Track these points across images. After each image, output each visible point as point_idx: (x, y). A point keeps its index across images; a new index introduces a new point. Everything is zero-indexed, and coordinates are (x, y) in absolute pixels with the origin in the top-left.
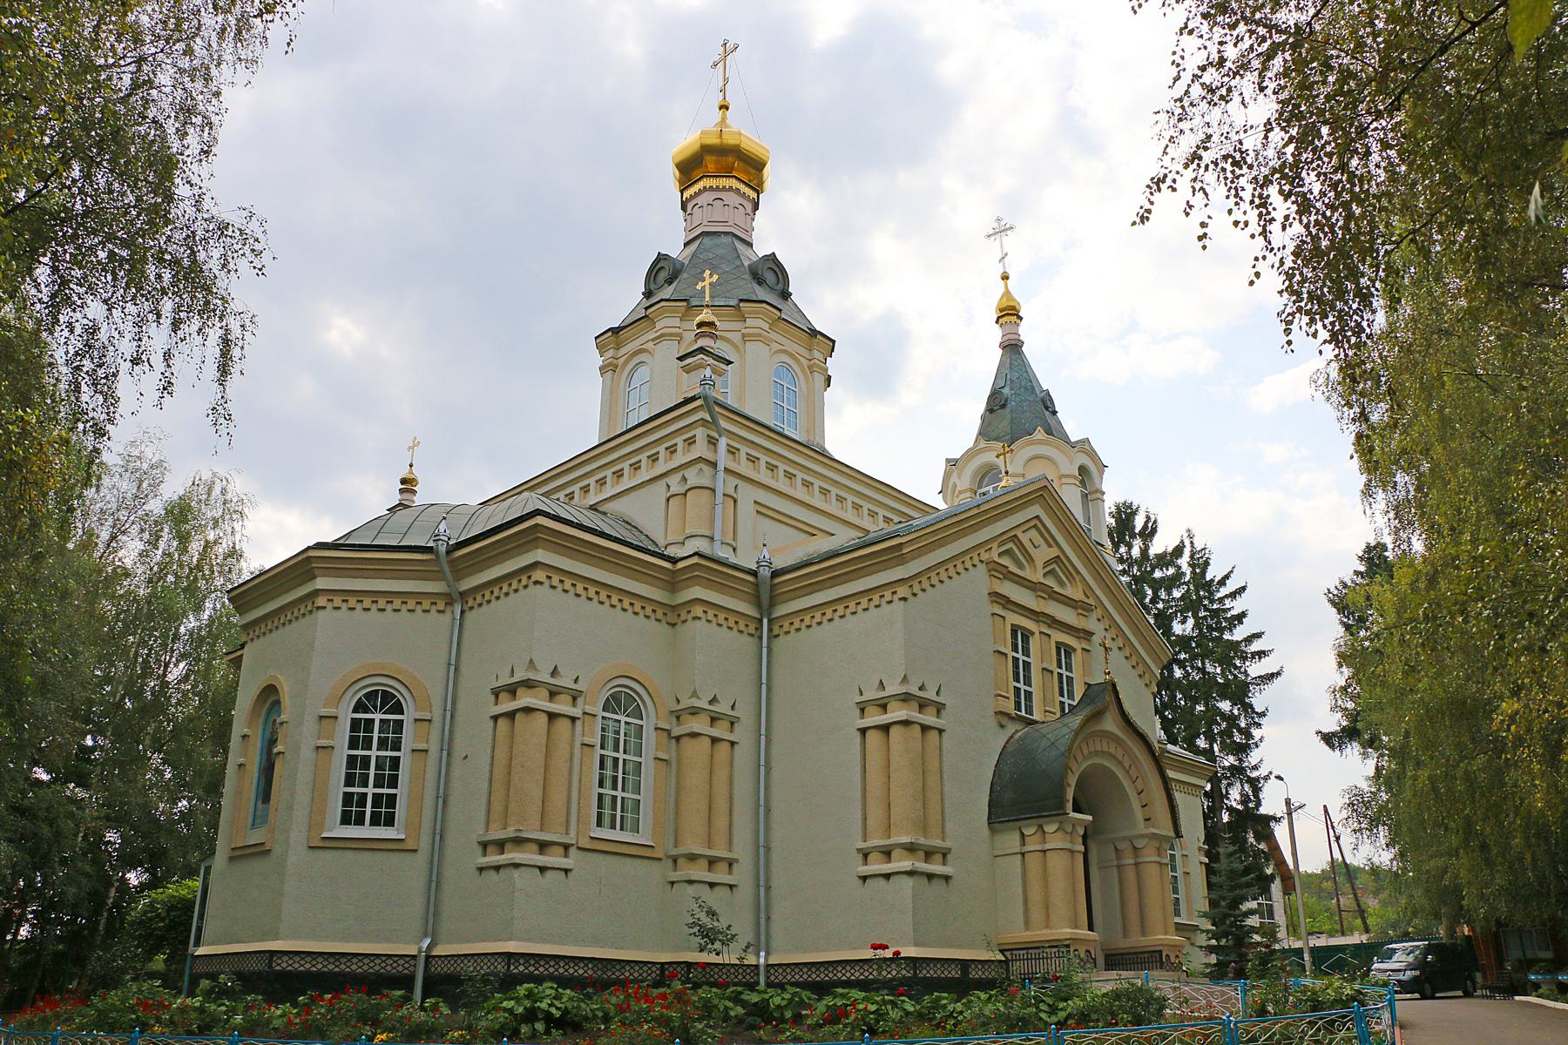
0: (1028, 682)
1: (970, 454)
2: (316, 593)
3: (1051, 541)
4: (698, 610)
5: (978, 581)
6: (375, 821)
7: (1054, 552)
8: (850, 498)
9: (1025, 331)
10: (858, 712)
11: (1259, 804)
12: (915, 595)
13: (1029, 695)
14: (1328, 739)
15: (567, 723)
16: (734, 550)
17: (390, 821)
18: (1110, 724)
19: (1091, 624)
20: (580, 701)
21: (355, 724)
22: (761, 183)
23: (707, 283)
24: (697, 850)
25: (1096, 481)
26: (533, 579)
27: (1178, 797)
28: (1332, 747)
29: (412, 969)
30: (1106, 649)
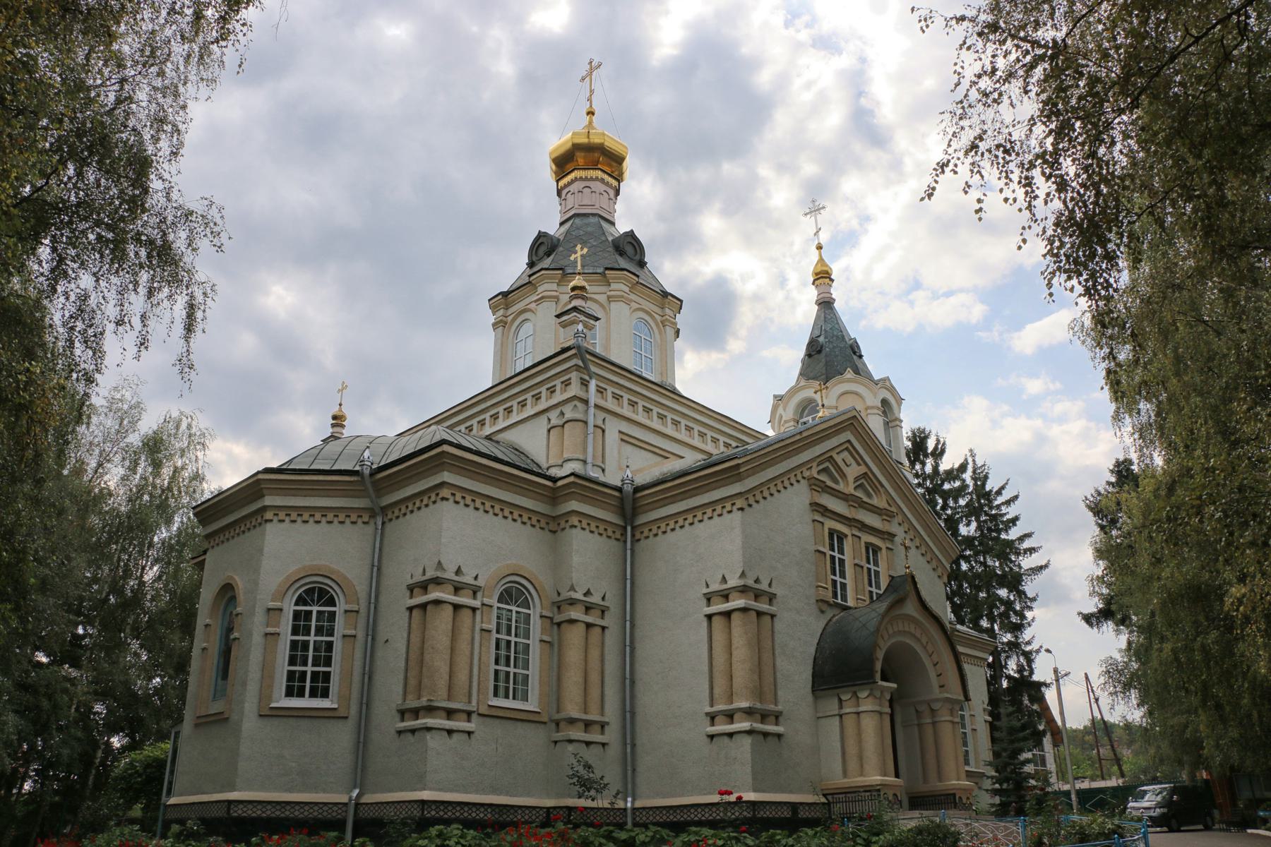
0: (843, 575)
1: (793, 391)
2: (265, 508)
3: (860, 461)
4: (574, 520)
5: (797, 498)
7: (863, 469)
8: (697, 428)
9: (836, 292)
10: (705, 601)
11: (1032, 672)
12: (750, 506)
13: (844, 586)
14: (1088, 619)
15: (469, 612)
16: (603, 470)
17: (325, 694)
18: (910, 608)
19: (894, 528)
20: (479, 595)
21: (297, 615)
25: (896, 411)
27: (966, 667)
28: (1091, 625)
30: (906, 548)
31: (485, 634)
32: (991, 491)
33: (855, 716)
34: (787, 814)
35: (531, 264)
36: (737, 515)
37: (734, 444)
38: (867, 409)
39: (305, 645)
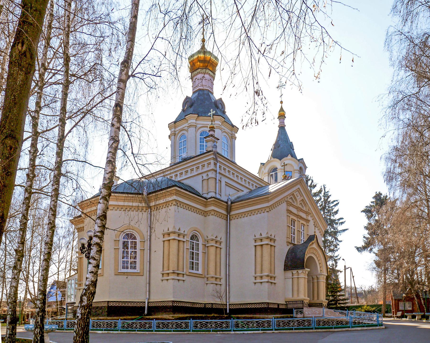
0: (294, 234)
3: (301, 195)
5: (284, 206)
7: (302, 198)
8: (248, 180)
10: (254, 241)
11: (336, 266)
14: (358, 249)
15: (183, 242)
16: (221, 195)
17: (135, 268)
18: (315, 246)
19: (310, 218)
20: (185, 237)
25: (304, 172)
28: (359, 251)
29: (144, 305)
32: (330, 201)
33: (297, 279)
34: (276, 307)
35: (183, 110)
36: (266, 214)
37: (258, 186)
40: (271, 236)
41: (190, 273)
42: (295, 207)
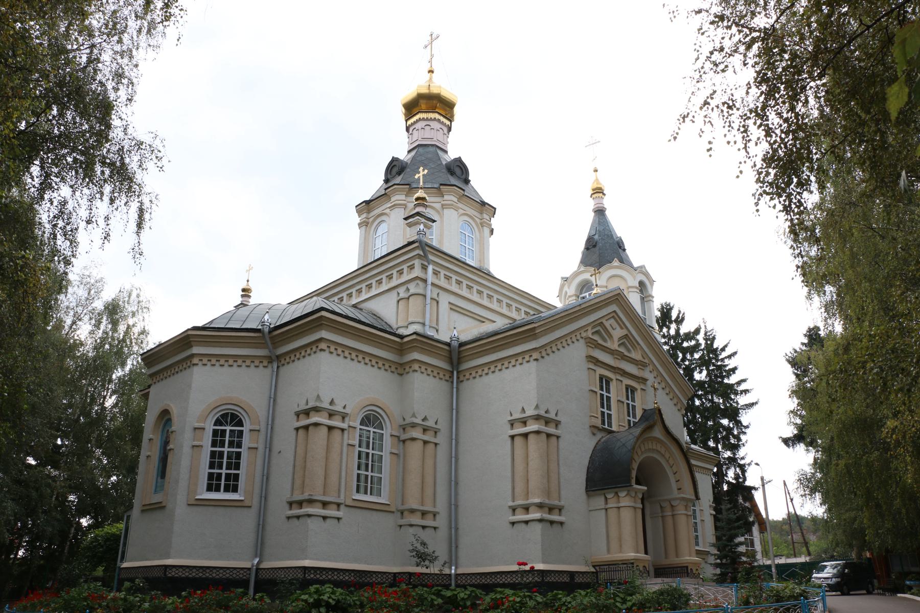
0: (609, 408)
1: (576, 274)
3: (622, 326)
4: (416, 366)
6: (227, 490)
7: (625, 332)
8: (505, 300)
9: (607, 203)
10: (509, 426)
11: (745, 479)
13: (609, 416)
14: (786, 441)
16: (437, 331)
17: (235, 489)
18: (657, 433)
19: (646, 374)
20: (347, 419)
21: (215, 433)
22: (452, 116)
23: (421, 174)
24: (415, 506)
26: (319, 348)
27: (698, 476)
28: (788, 446)
29: (248, 576)
30: (655, 389)
31: (350, 448)
34: (566, 579)
35: (387, 181)
36: (533, 364)
37: (532, 313)
38: (629, 287)
39: (221, 454)
40: (547, 412)
41: (356, 502)
42: (608, 350)
